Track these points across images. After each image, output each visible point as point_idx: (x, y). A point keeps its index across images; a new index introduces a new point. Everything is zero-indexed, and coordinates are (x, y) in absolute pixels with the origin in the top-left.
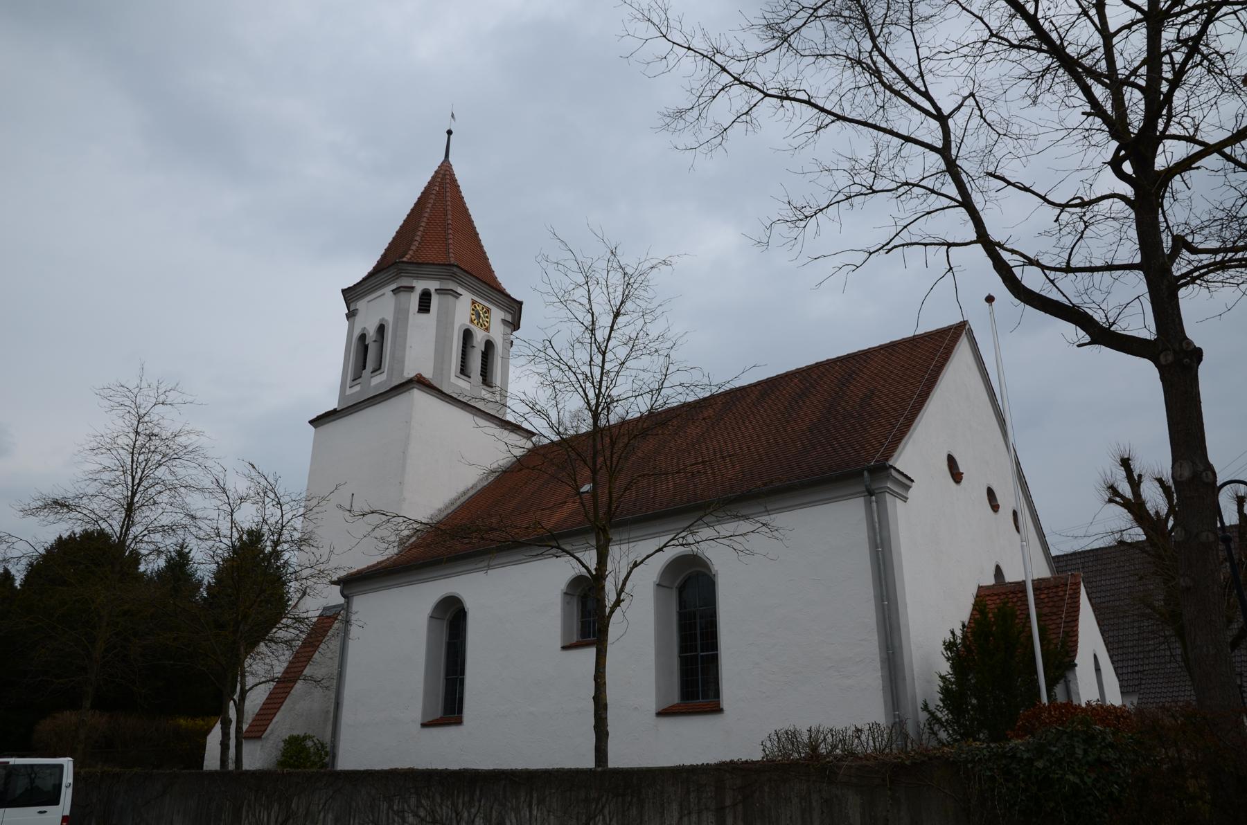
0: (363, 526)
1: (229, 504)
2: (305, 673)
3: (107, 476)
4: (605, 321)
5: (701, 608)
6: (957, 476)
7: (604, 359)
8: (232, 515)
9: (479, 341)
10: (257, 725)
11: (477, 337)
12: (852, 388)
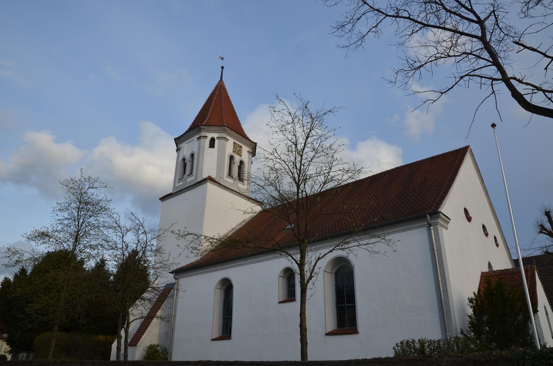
0: (183, 242)
1: (122, 233)
2: (157, 314)
3: (66, 222)
4: (301, 141)
5: (346, 283)
6: (469, 219)
7: (301, 158)
8: (123, 238)
9: (237, 161)
10: (135, 340)
11: (236, 159)
12: (415, 178)
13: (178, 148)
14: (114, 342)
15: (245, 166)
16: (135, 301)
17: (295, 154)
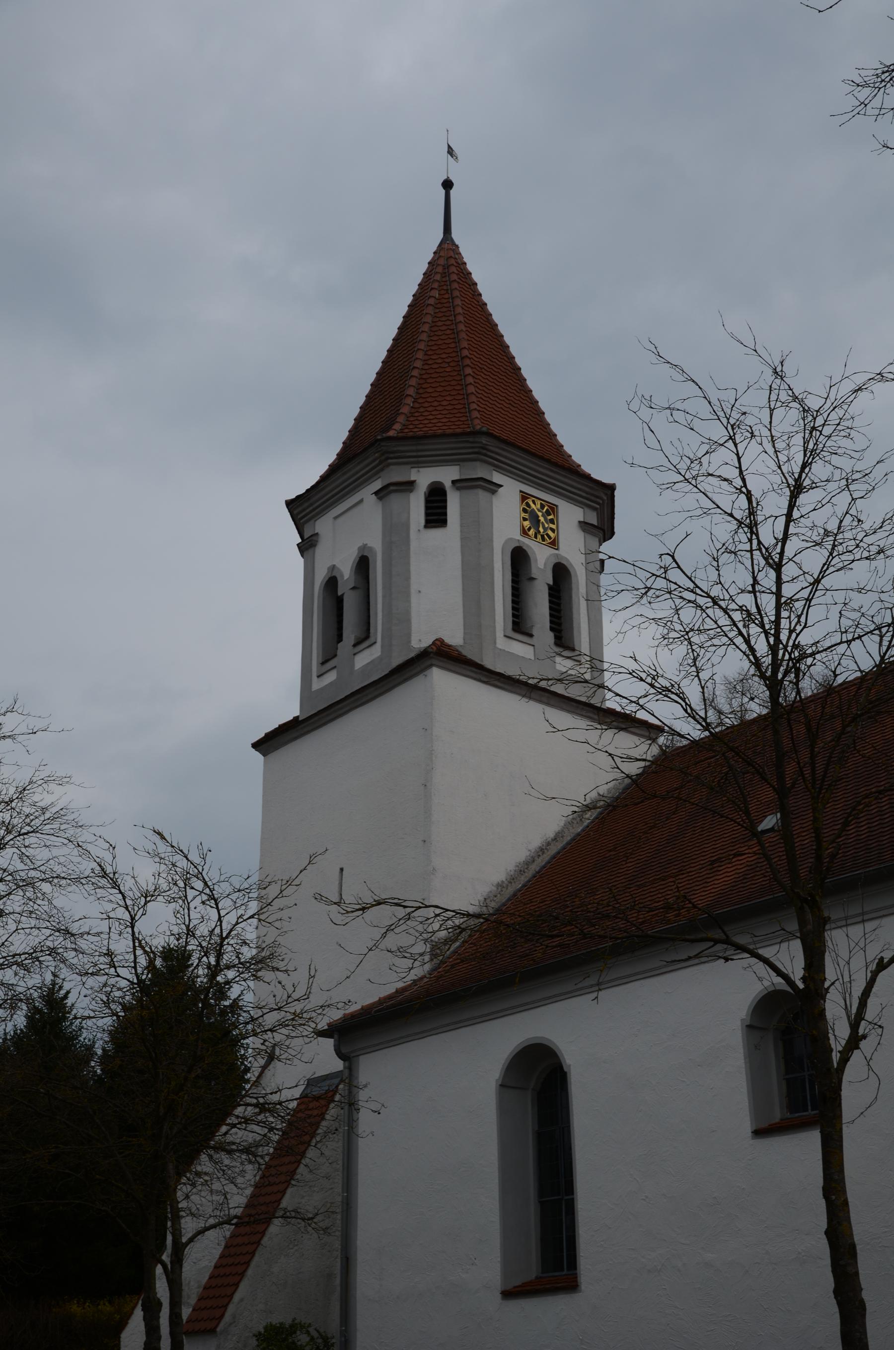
1: (127, 908)
2: (284, 1203)
8: (133, 927)
11: (536, 560)
13: (306, 537)
14: (126, 1323)
15: (574, 586)
16: (192, 1157)
17: (753, 568)
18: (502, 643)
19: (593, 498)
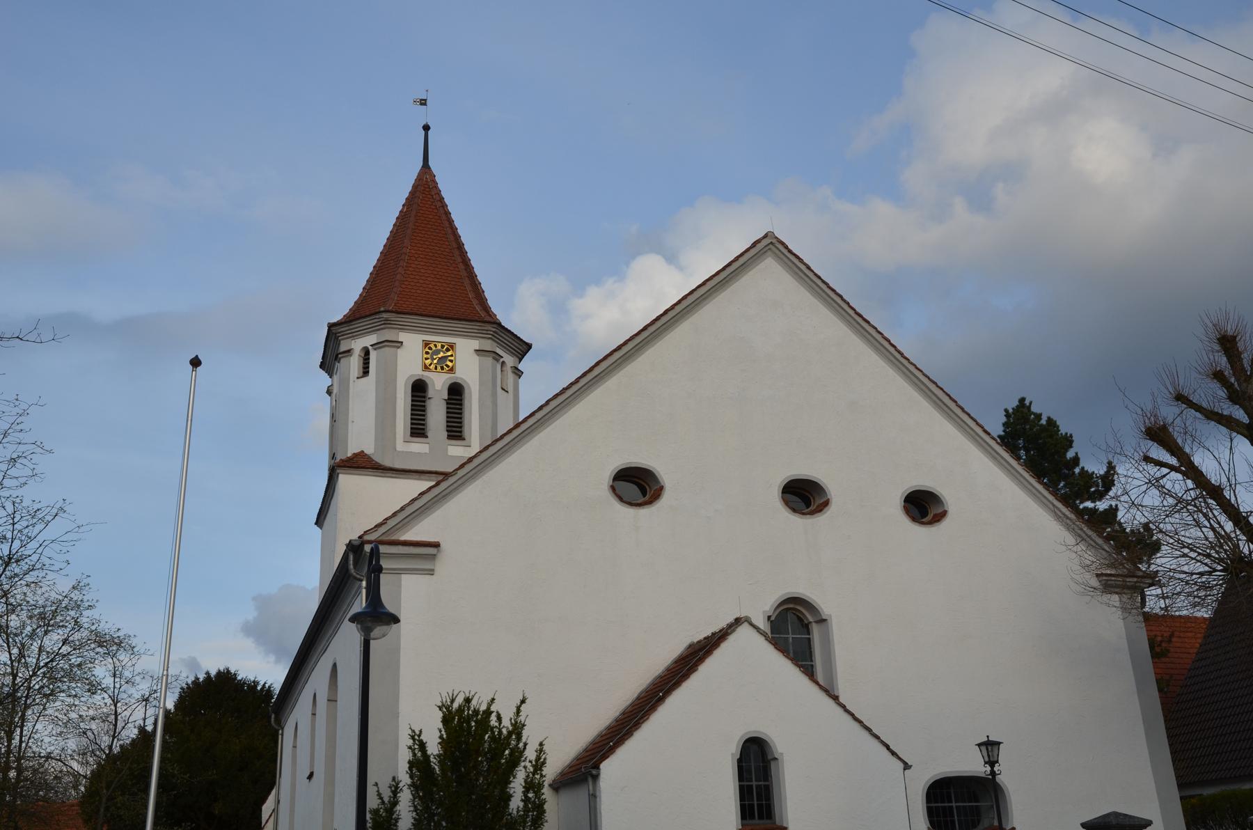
18: (400, 446)
19: (484, 332)
